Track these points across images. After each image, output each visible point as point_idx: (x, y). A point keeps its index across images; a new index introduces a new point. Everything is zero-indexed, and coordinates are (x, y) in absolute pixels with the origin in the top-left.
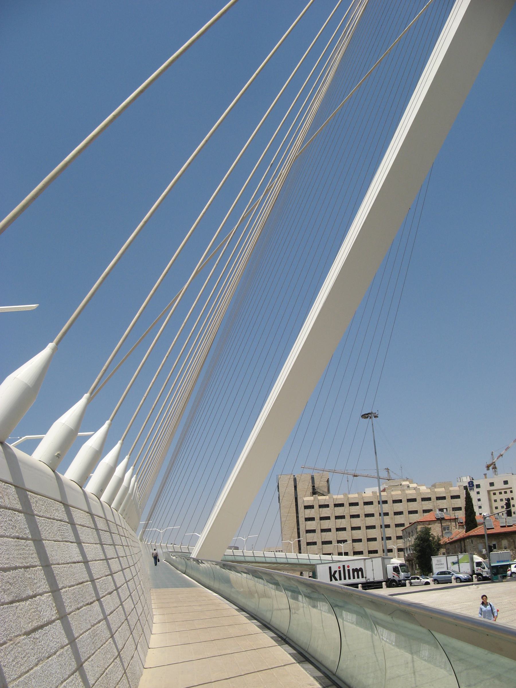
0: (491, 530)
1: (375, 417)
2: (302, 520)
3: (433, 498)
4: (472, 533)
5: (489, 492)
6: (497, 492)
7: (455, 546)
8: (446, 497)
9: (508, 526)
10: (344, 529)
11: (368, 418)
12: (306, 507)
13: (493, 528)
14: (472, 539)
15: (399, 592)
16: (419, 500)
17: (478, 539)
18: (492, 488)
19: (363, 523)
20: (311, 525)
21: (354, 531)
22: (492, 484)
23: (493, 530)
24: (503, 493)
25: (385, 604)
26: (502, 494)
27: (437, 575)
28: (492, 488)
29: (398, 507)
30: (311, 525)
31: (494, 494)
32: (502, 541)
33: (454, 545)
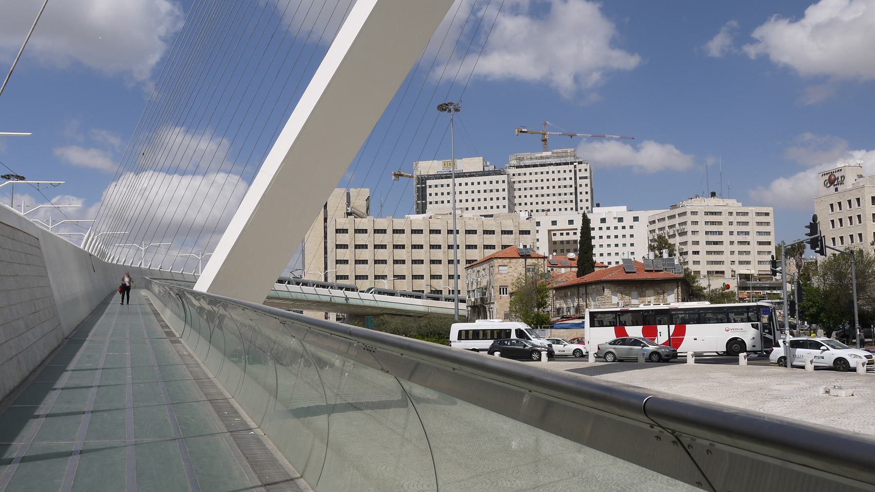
0: (632, 274)
1: (457, 110)
2: (331, 246)
3: (498, 231)
4: (587, 278)
5: (549, 231)
6: (558, 233)
7: (564, 293)
8: (514, 232)
9: (656, 271)
10: (346, 262)
11: (446, 110)
12: (338, 231)
13: (635, 272)
14: (605, 285)
15: (700, 366)
16: (480, 232)
17: (613, 285)
18: (554, 227)
19: (408, 255)
20: (342, 254)
21: (396, 266)
22: (554, 223)
23: (634, 274)
24: (565, 234)
25: (400, 355)
26: (563, 235)
27: (263, 304)
28: (554, 227)
29: (418, 239)
30: (342, 254)
31: (555, 235)
32: (647, 291)
33: (564, 291)
